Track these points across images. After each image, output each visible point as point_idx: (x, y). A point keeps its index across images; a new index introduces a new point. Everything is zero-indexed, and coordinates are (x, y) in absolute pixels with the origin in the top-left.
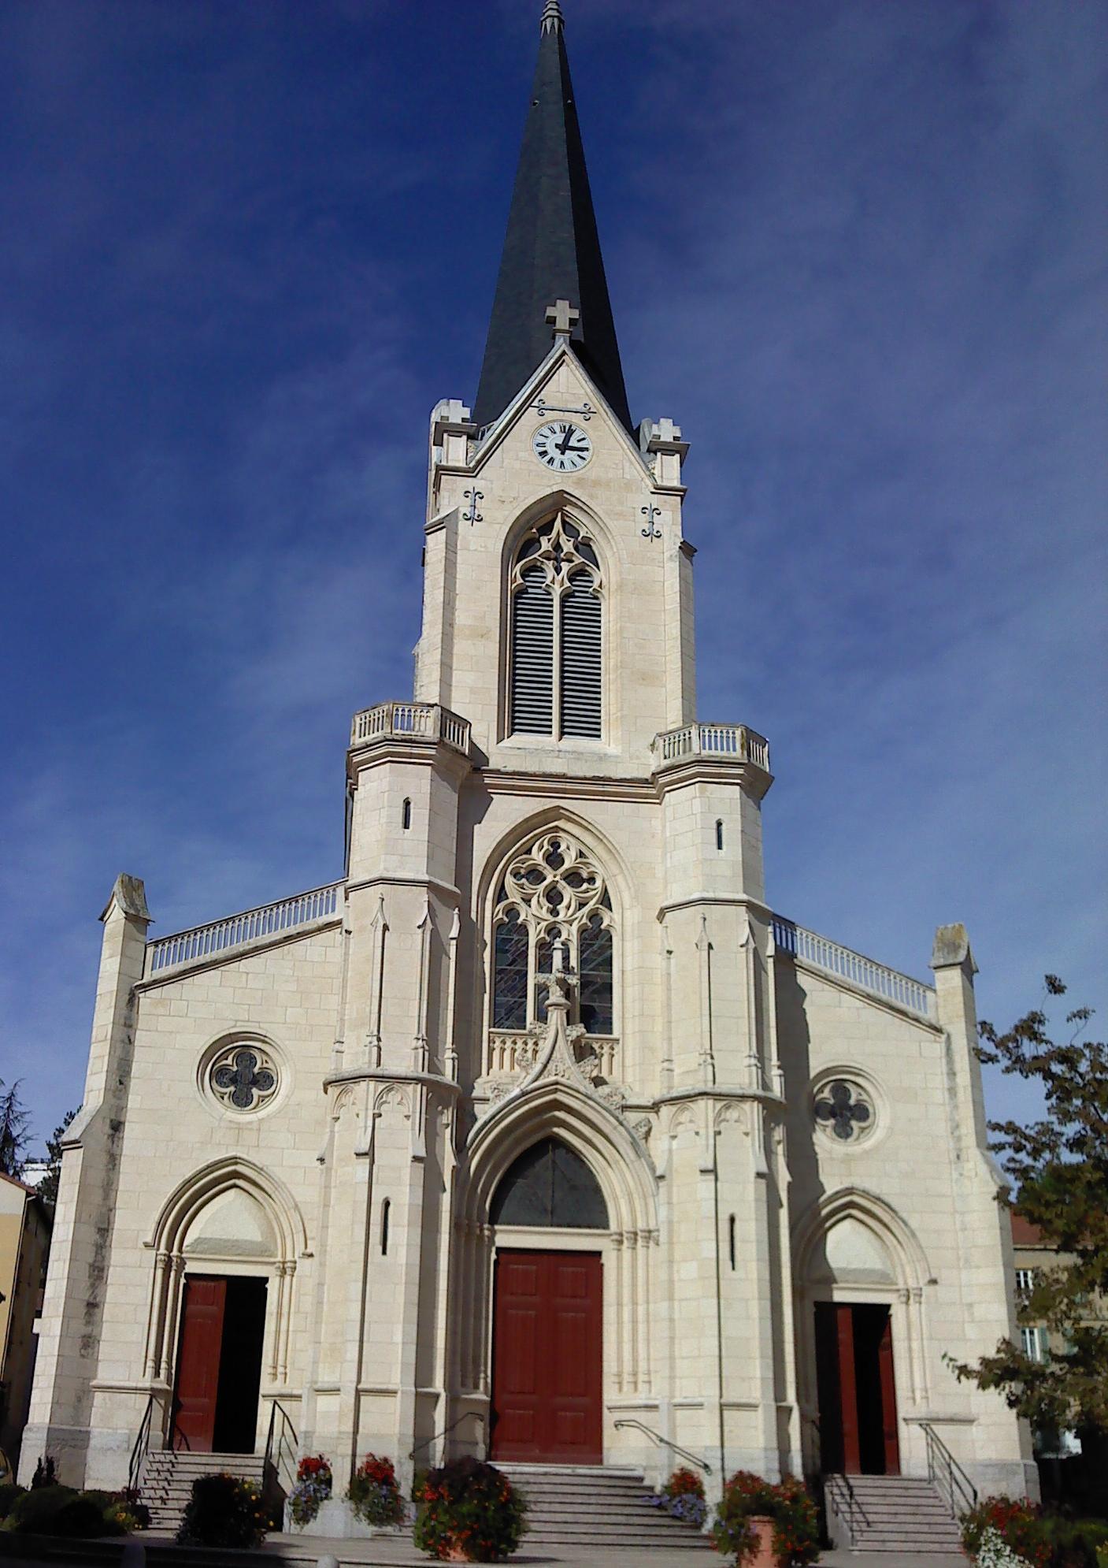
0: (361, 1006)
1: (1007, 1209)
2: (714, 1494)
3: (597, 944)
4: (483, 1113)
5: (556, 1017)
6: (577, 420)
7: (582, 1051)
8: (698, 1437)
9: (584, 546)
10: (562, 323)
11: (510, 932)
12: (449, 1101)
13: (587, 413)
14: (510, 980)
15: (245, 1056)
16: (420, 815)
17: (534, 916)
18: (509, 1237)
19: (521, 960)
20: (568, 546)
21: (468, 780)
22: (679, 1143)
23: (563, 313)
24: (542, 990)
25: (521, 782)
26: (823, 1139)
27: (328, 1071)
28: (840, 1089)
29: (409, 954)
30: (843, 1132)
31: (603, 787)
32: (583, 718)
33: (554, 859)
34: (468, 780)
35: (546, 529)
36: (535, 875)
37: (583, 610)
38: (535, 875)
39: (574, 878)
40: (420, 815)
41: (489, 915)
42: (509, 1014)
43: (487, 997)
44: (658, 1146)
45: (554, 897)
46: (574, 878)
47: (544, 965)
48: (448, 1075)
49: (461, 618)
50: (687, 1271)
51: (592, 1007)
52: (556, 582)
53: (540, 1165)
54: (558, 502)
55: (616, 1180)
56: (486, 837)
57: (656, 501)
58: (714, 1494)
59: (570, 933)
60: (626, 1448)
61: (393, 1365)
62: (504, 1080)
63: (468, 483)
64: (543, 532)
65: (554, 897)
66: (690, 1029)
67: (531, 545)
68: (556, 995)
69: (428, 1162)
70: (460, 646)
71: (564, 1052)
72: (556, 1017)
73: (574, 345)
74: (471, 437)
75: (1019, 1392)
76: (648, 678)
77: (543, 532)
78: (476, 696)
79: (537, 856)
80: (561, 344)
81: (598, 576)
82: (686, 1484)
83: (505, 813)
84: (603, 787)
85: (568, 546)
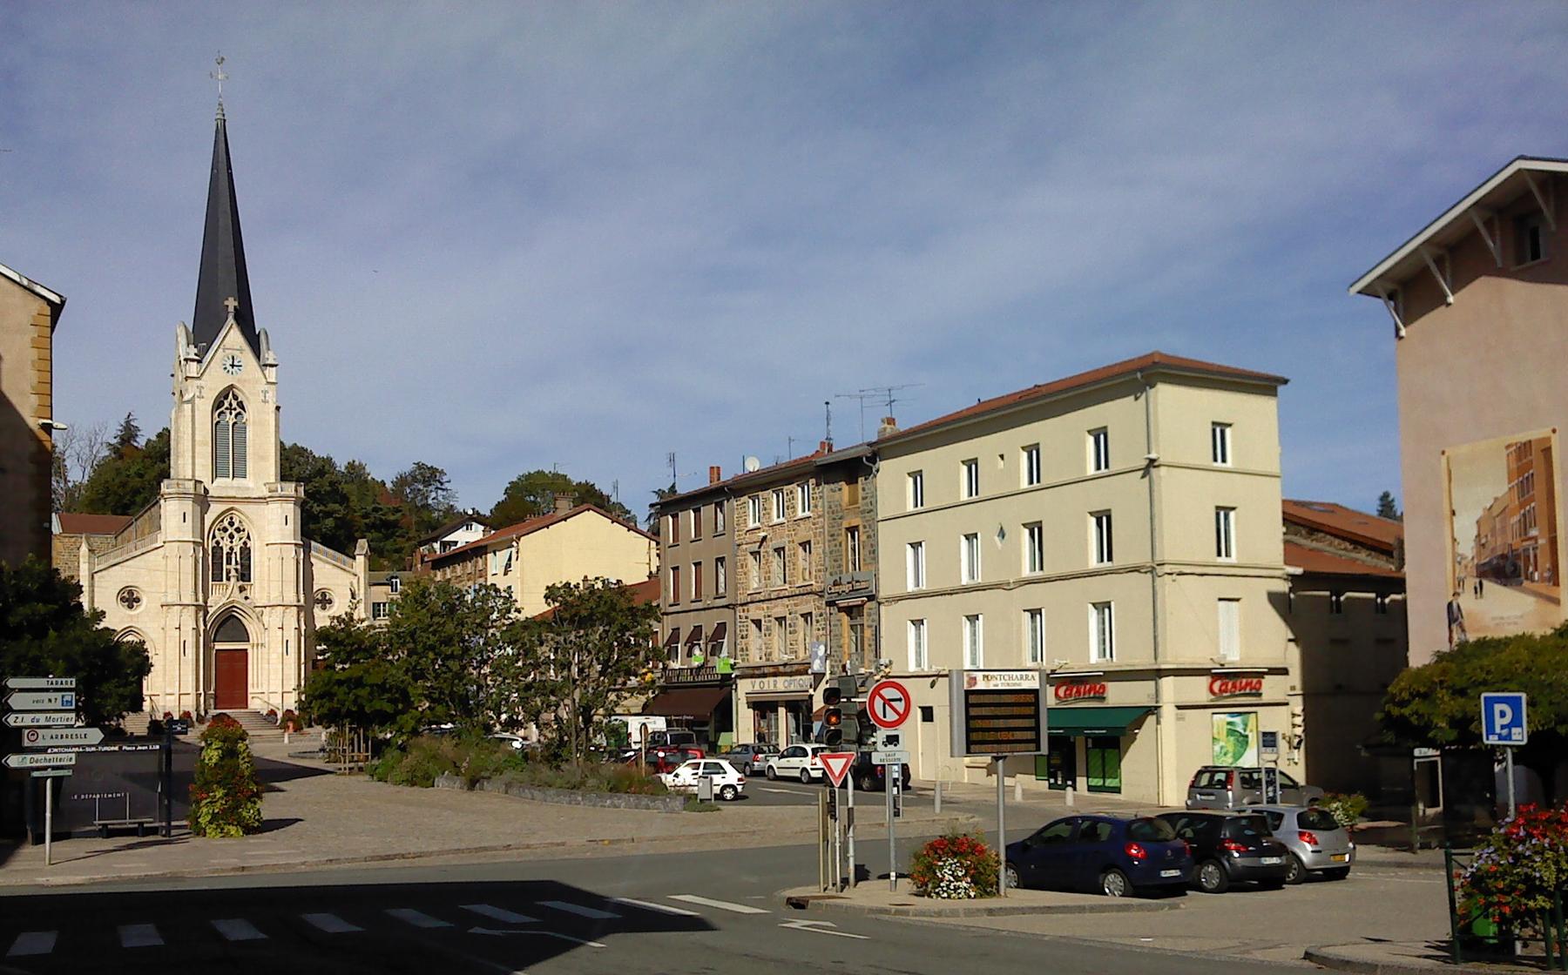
0: (172, 581)
1: (868, 451)
2: (280, 715)
3: (246, 552)
4: (211, 611)
5: (233, 580)
6: (236, 353)
7: (242, 589)
8: (275, 701)
9: (240, 404)
10: (231, 309)
11: (217, 549)
12: (202, 609)
13: (241, 350)
14: (217, 566)
15: (131, 593)
16: (189, 518)
17: (225, 545)
18: (219, 646)
19: (223, 560)
20: (234, 404)
21: (203, 500)
22: (272, 618)
23: (232, 303)
24: (228, 572)
25: (220, 499)
26: (317, 610)
27: (163, 601)
28: (324, 594)
29: (188, 564)
30: (324, 608)
31: (248, 500)
32: (239, 472)
33: (232, 524)
34: (203, 500)
35: (226, 397)
36: (225, 530)
37: (240, 429)
38: (225, 530)
39: (238, 530)
40: (189, 518)
41: (212, 544)
42: (217, 578)
43: (484, 931)
44: (265, 619)
45: (231, 536)
46: (238, 530)
47: (229, 563)
48: (201, 602)
49: (197, 438)
50: (274, 656)
51: (245, 575)
52: (230, 418)
53: (229, 624)
54: (232, 386)
55: (252, 627)
56: (209, 518)
57: (267, 387)
58: (280, 715)
59: (237, 549)
60: (255, 704)
61: (189, 685)
62: (218, 599)
63: (198, 382)
64: (227, 401)
65: (231, 536)
66: (276, 586)
67: (220, 404)
68: (233, 573)
69: (197, 629)
70: (197, 449)
71: (236, 590)
72: (233, 580)
73: (236, 318)
74: (199, 362)
75: (1480, 921)
76: (263, 458)
77: (227, 401)
78: (204, 474)
79: (226, 523)
80: (231, 320)
81: (246, 416)
82: (272, 713)
83: (215, 509)
84: (248, 500)
85: (234, 404)
